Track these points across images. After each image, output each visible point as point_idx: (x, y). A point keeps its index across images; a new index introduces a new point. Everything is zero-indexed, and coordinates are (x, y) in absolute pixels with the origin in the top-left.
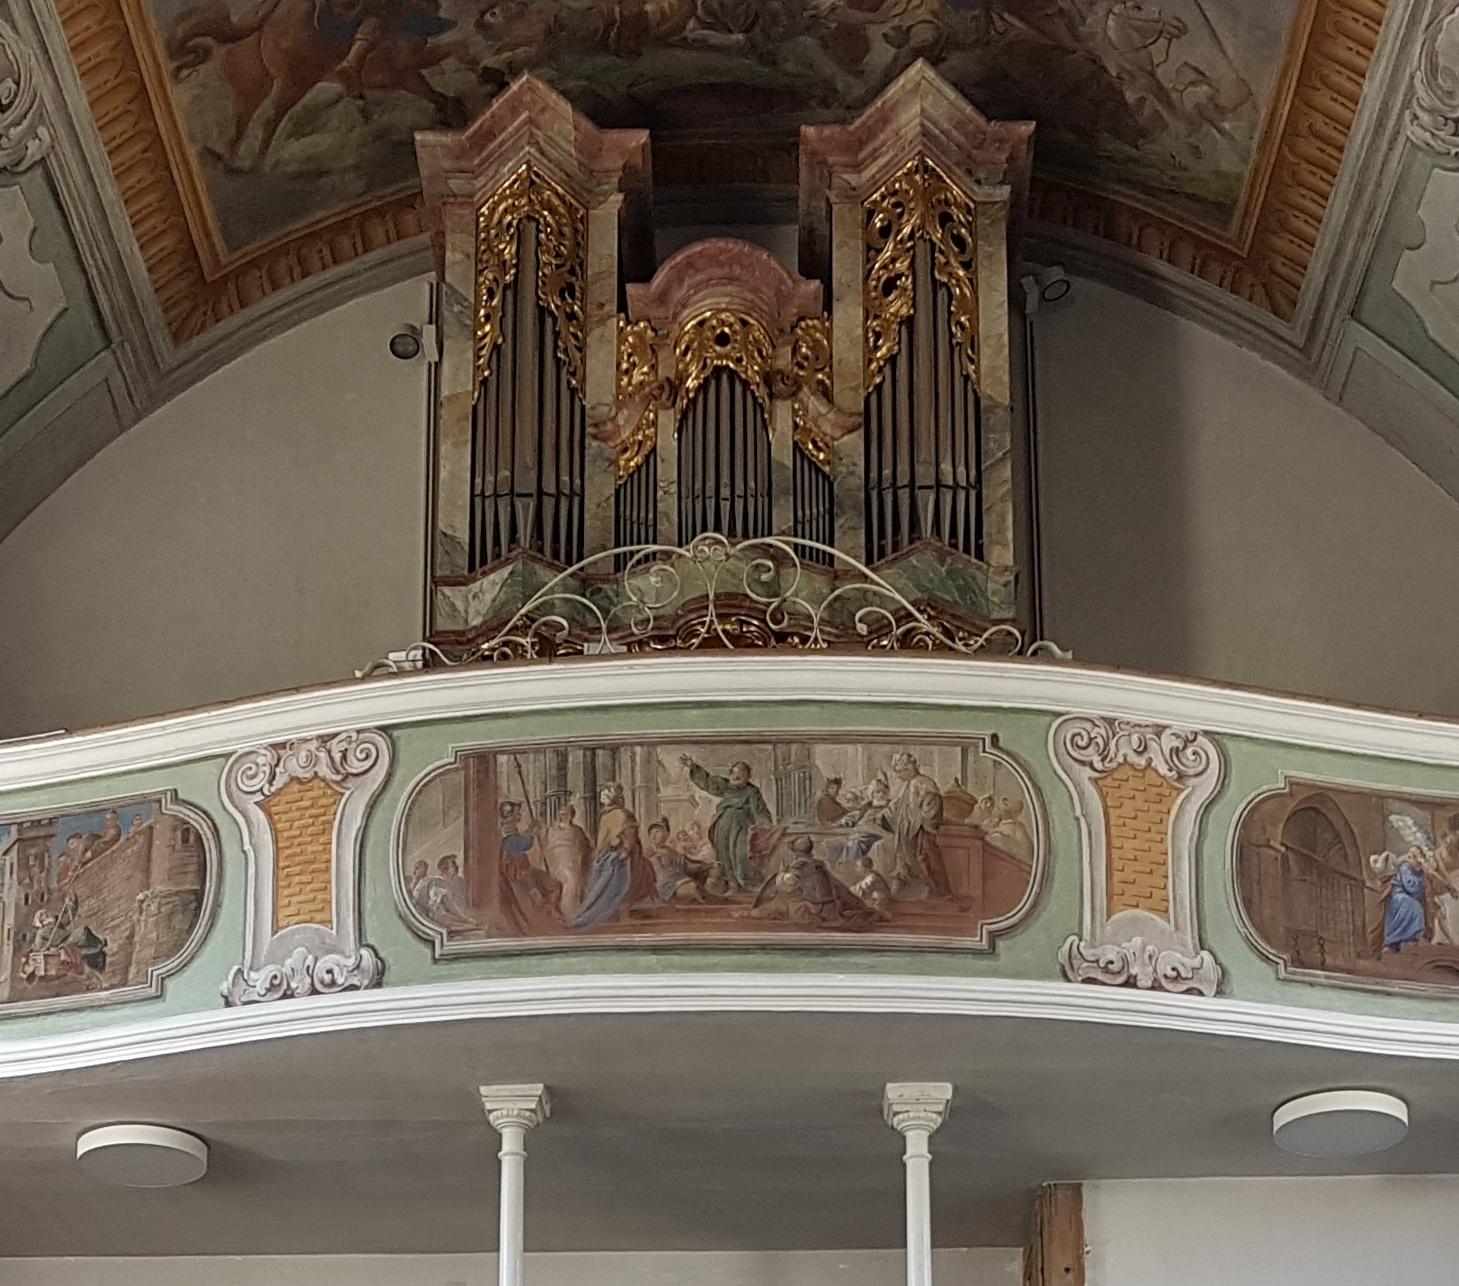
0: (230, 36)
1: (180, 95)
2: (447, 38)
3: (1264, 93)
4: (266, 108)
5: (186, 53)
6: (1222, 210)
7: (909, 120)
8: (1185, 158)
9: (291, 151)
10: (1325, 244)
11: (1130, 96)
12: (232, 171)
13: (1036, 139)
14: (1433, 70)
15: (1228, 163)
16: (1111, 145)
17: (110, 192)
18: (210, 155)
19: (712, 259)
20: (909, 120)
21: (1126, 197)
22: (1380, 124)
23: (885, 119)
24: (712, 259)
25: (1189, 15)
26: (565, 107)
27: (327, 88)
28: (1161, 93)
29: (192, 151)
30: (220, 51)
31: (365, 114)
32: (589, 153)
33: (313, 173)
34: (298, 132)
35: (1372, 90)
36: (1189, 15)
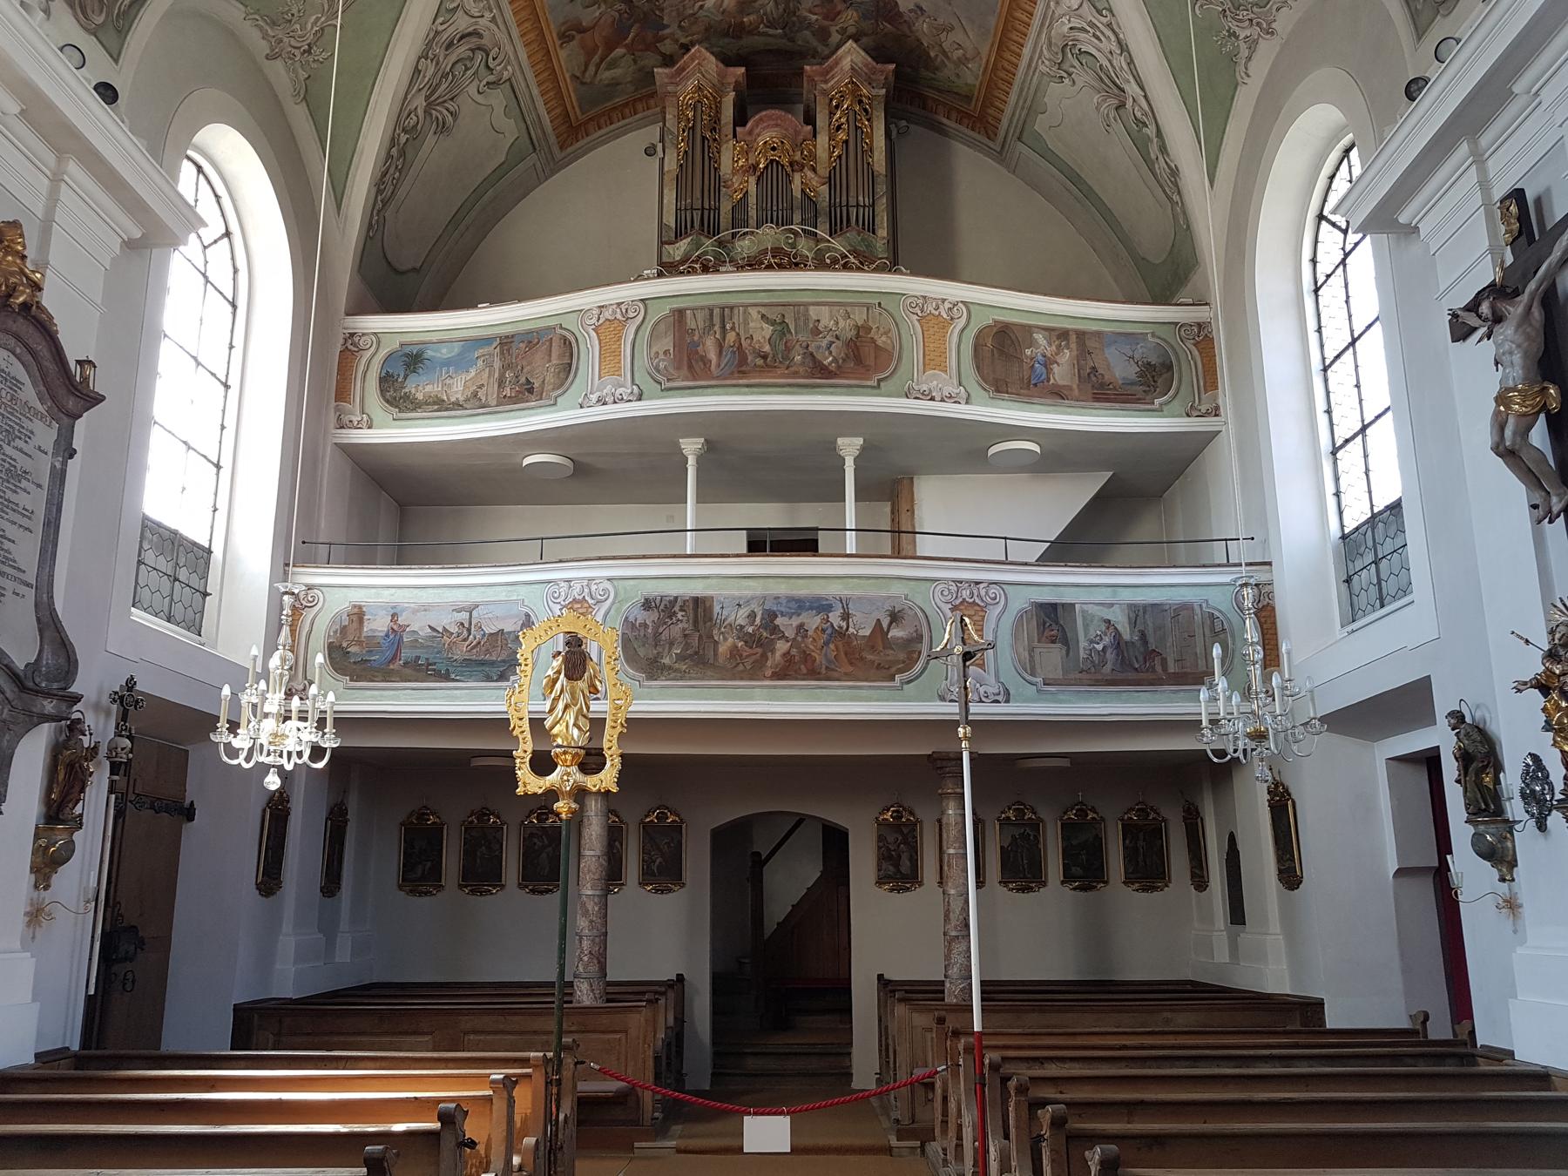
0: (582, 31)
1: (563, 54)
2: (667, 31)
3: (984, 52)
4: (596, 58)
5: (565, 37)
6: (968, 98)
7: (846, 64)
8: (953, 78)
9: (606, 75)
10: (1008, 111)
11: (932, 54)
12: (583, 83)
13: (896, 71)
14: (1050, 44)
15: (970, 80)
16: (924, 73)
17: (535, 92)
18: (574, 77)
19: (770, 118)
20: (846, 64)
21: (931, 93)
22: (1029, 65)
23: (837, 63)
24: (770, 118)
25: (955, 23)
26: (713, 59)
27: (620, 51)
28: (944, 53)
29: (567, 76)
30: (578, 37)
31: (635, 61)
32: (722, 76)
33: (614, 84)
34: (608, 69)
35: (1026, 51)
36: (955, 23)
